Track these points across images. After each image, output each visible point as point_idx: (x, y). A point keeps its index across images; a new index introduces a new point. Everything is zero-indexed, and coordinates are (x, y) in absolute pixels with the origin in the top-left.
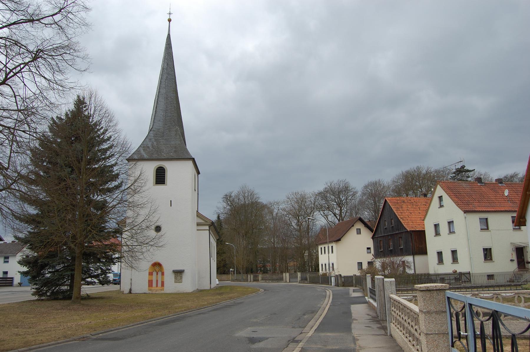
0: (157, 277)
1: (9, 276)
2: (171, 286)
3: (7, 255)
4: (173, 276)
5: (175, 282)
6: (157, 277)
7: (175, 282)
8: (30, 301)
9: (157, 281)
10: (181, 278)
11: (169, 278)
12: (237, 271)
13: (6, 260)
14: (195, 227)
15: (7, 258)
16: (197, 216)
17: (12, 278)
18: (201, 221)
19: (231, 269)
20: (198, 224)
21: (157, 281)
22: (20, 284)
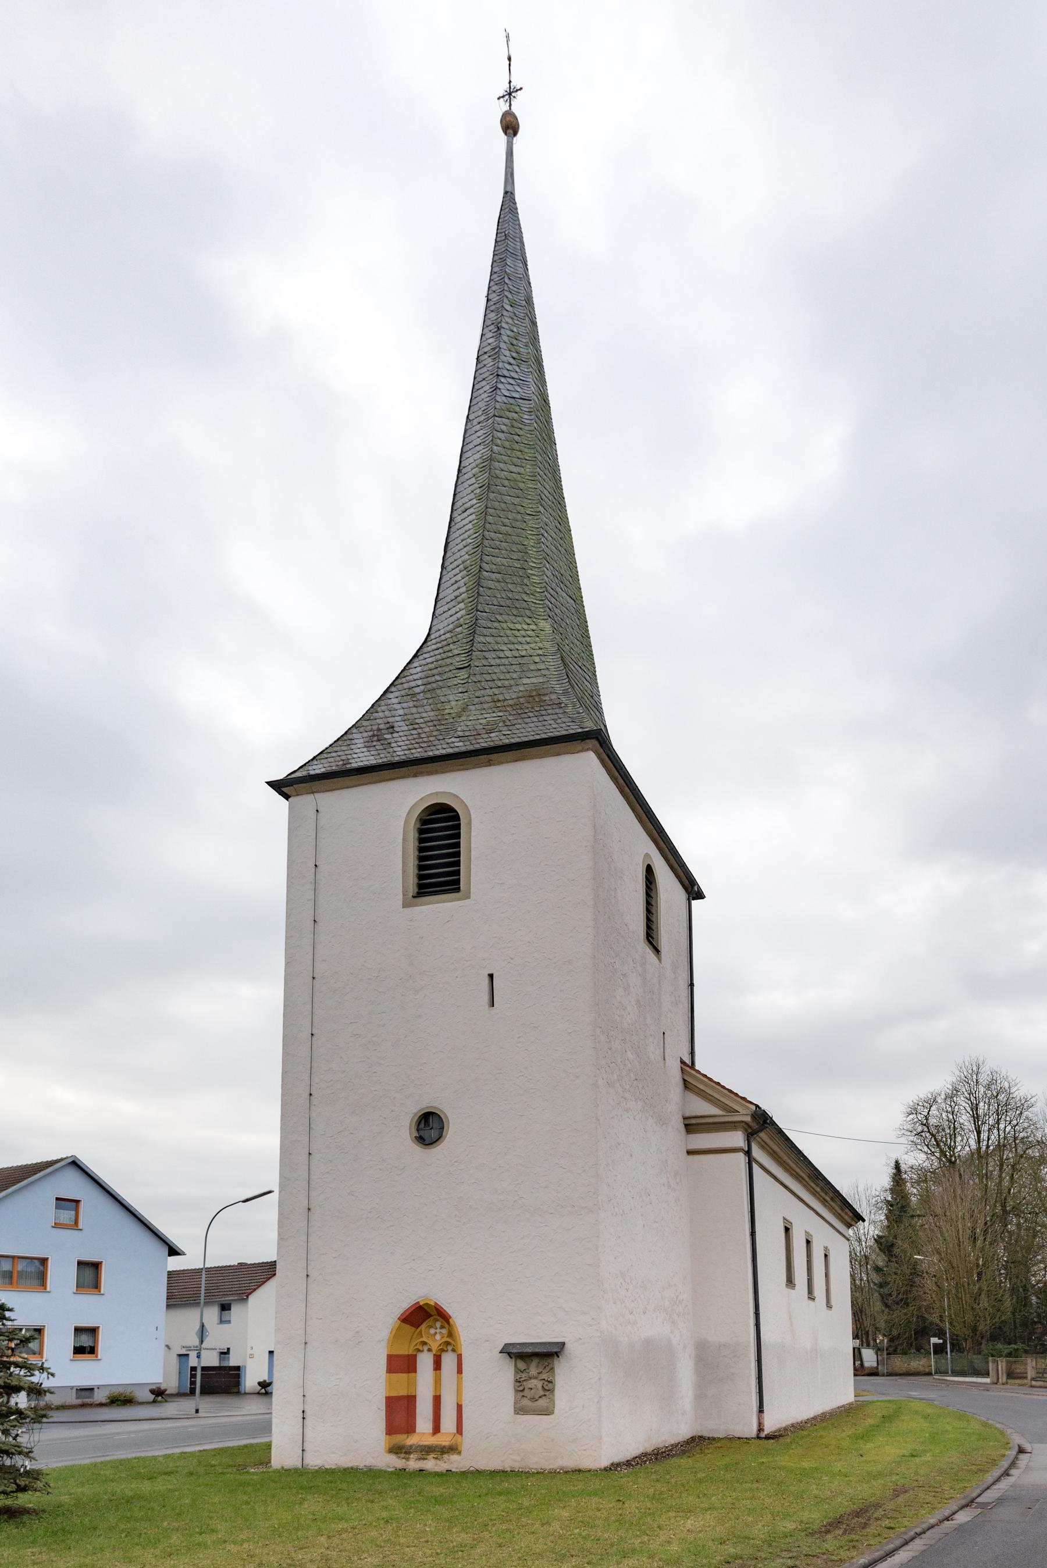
0: (438, 1382)
1: (233, 1362)
2: (489, 1423)
3: (226, 1299)
4: (505, 1373)
5: (520, 1410)
6: (438, 1382)
7: (520, 1410)
8: (372, 1473)
9: (437, 1400)
10: (548, 1388)
11: (484, 1390)
12: (952, 1344)
13: (85, 1341)
14: (674, 1136)
15: (225, 1308)
16: (687, 1085)
17: (238, 1368)
18: (702, 1108)
19: (934, 1340)
20: (692, 1125)
21: (437, 1400)
22: (1033, 1379)
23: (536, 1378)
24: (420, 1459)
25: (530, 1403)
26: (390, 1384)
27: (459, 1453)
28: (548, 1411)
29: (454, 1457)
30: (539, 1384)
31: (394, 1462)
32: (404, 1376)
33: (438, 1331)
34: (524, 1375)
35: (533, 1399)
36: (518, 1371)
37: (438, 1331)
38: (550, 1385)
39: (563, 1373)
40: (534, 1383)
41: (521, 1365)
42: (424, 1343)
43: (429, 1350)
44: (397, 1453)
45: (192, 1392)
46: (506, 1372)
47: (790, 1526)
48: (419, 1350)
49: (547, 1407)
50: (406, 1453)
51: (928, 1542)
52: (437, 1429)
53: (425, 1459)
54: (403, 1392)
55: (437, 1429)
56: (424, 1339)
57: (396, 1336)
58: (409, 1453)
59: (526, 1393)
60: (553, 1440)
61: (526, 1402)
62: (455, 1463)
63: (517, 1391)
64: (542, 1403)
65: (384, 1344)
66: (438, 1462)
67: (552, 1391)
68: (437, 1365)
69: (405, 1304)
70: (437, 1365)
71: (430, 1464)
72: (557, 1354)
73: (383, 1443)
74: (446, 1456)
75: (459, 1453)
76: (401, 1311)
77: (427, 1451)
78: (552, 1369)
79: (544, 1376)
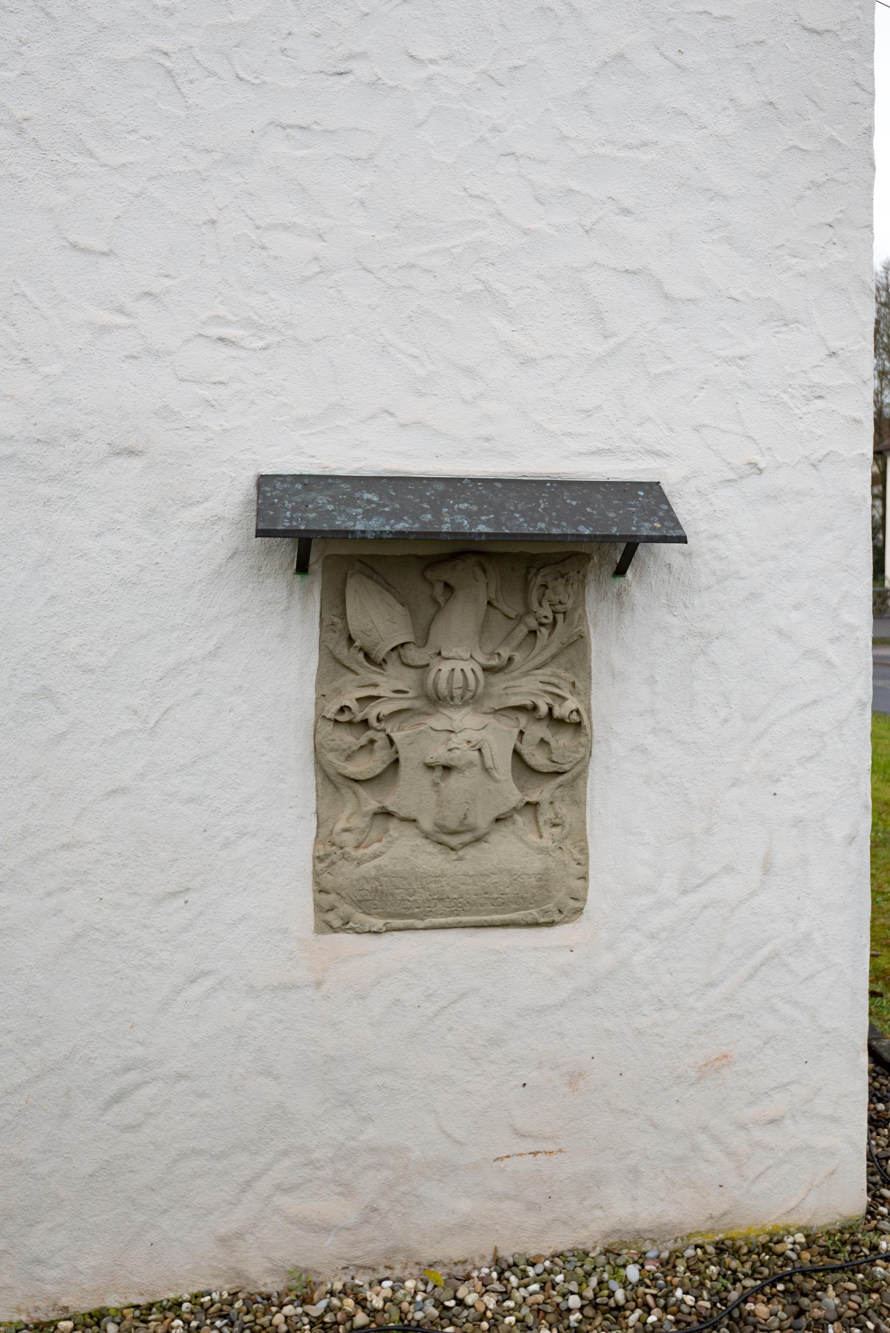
5: (351, 903)
7: (351, 903)
10: (551, 757)
23: (471, 699)
25: (430, 860)
28: (546, 904)
30: (499, 738)
34: (390, 682)
35: (454, 836)
36: (343, 650)
38: (562, 740)
39: (639, 659)
40: (468, 730)
41: (378, 617)
45: (687, 1237)
46: (267, 663)
47: (792, 326)
49: (544, 879)
51: (617, 1286)
59: (411, 793)
60: (574, 1079)
61: (404, 853)
63: (332, 781)
64: (514, 853)
67: (568, 777)
72: (625, 555)
78: (578, 643)
79: (526, 688)
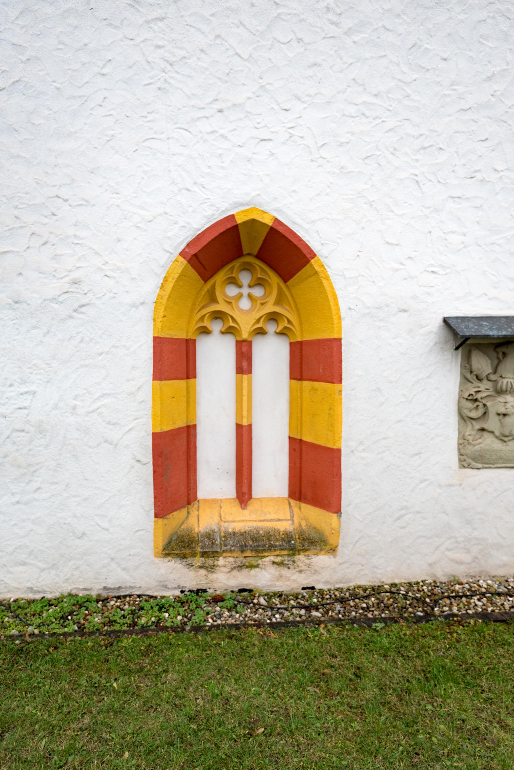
0: (243, 398)
6: (243, 398)
7: (471, 459)
9: (244, 435)
21: (244, 435)
24: (240, 568)
25: (497, 445)
26: (159, 399)
27: (333, 550)
29: (321, 560)
31: (173, 577)
32: (182, 383)
33: (245, 291)
37: (245, 291)
41: (482, 363)
42: (218, 316)
43: (229, 331)
44: (184, 557)
48: (205, 331)
50: (204, 554)
52: (244, 493)
53: (251, 567)
54: (181, 423)
55: (244, 493)
56: (221, 307)
57: (173, 298)
58: (215, 555)
59: (492, 423)
62: (324, 572)
65: (146, 314)
66: (285, 571)
68: (244, 362)
69: (199, 218)
70: (244, 362)
71: (267, 577)
73: (149, 536)
74: (301, 558)
75: (333, 550)
76: (189, 235)
77: (255, 545)
